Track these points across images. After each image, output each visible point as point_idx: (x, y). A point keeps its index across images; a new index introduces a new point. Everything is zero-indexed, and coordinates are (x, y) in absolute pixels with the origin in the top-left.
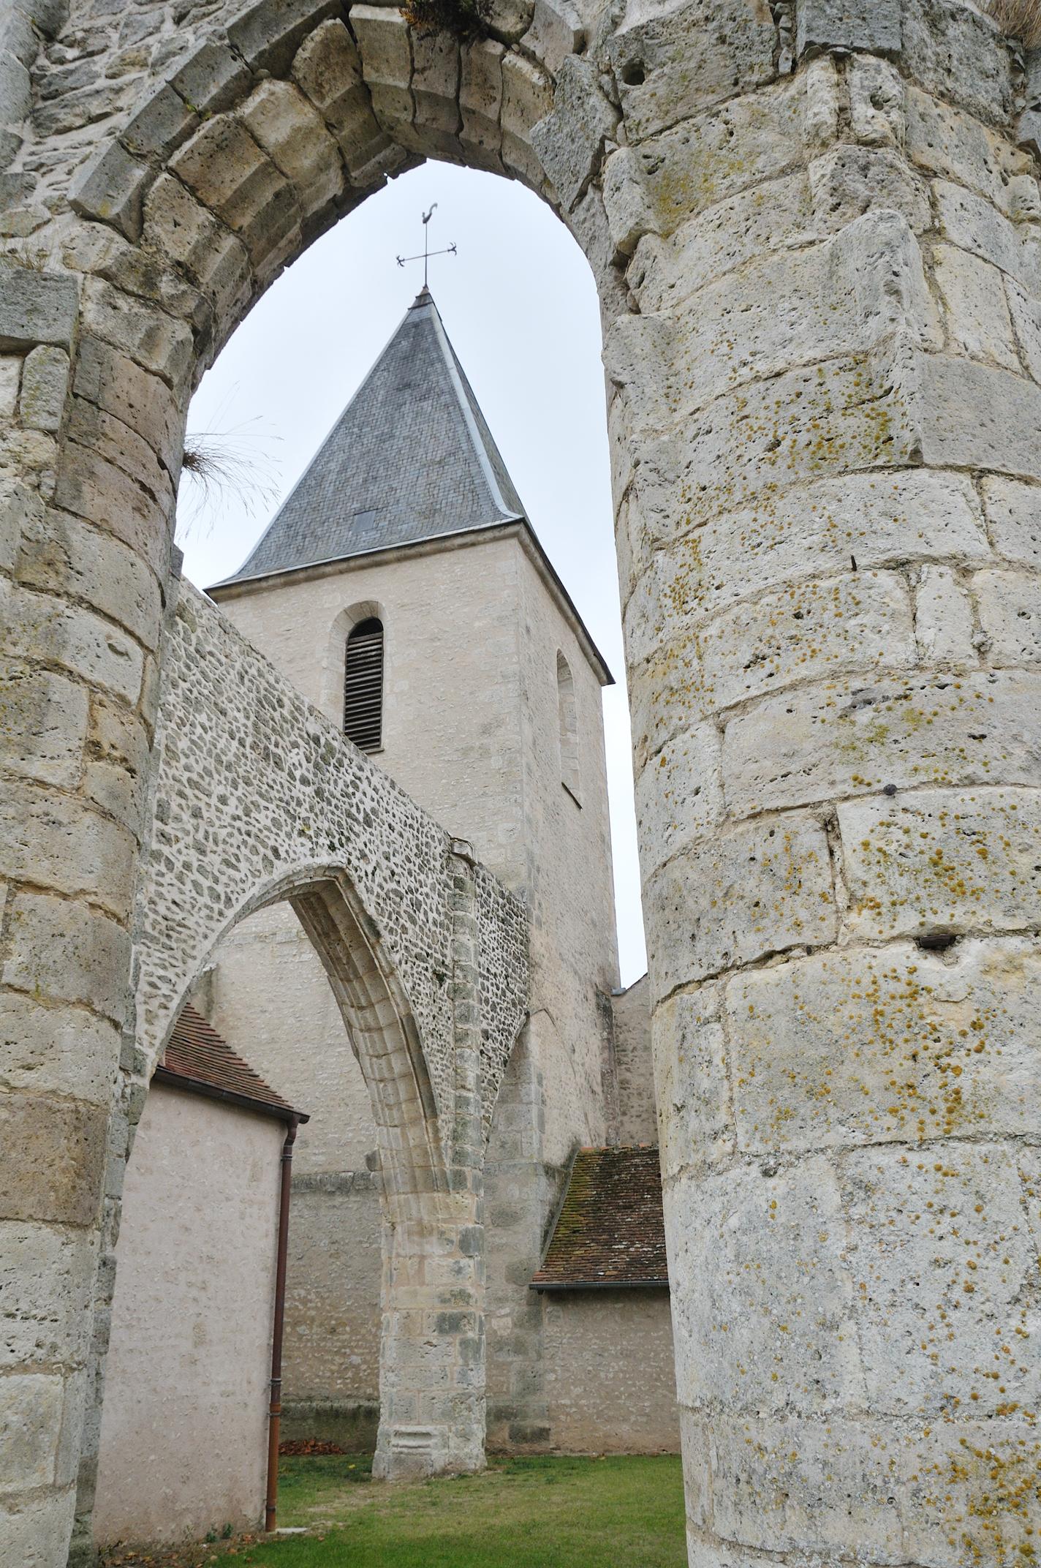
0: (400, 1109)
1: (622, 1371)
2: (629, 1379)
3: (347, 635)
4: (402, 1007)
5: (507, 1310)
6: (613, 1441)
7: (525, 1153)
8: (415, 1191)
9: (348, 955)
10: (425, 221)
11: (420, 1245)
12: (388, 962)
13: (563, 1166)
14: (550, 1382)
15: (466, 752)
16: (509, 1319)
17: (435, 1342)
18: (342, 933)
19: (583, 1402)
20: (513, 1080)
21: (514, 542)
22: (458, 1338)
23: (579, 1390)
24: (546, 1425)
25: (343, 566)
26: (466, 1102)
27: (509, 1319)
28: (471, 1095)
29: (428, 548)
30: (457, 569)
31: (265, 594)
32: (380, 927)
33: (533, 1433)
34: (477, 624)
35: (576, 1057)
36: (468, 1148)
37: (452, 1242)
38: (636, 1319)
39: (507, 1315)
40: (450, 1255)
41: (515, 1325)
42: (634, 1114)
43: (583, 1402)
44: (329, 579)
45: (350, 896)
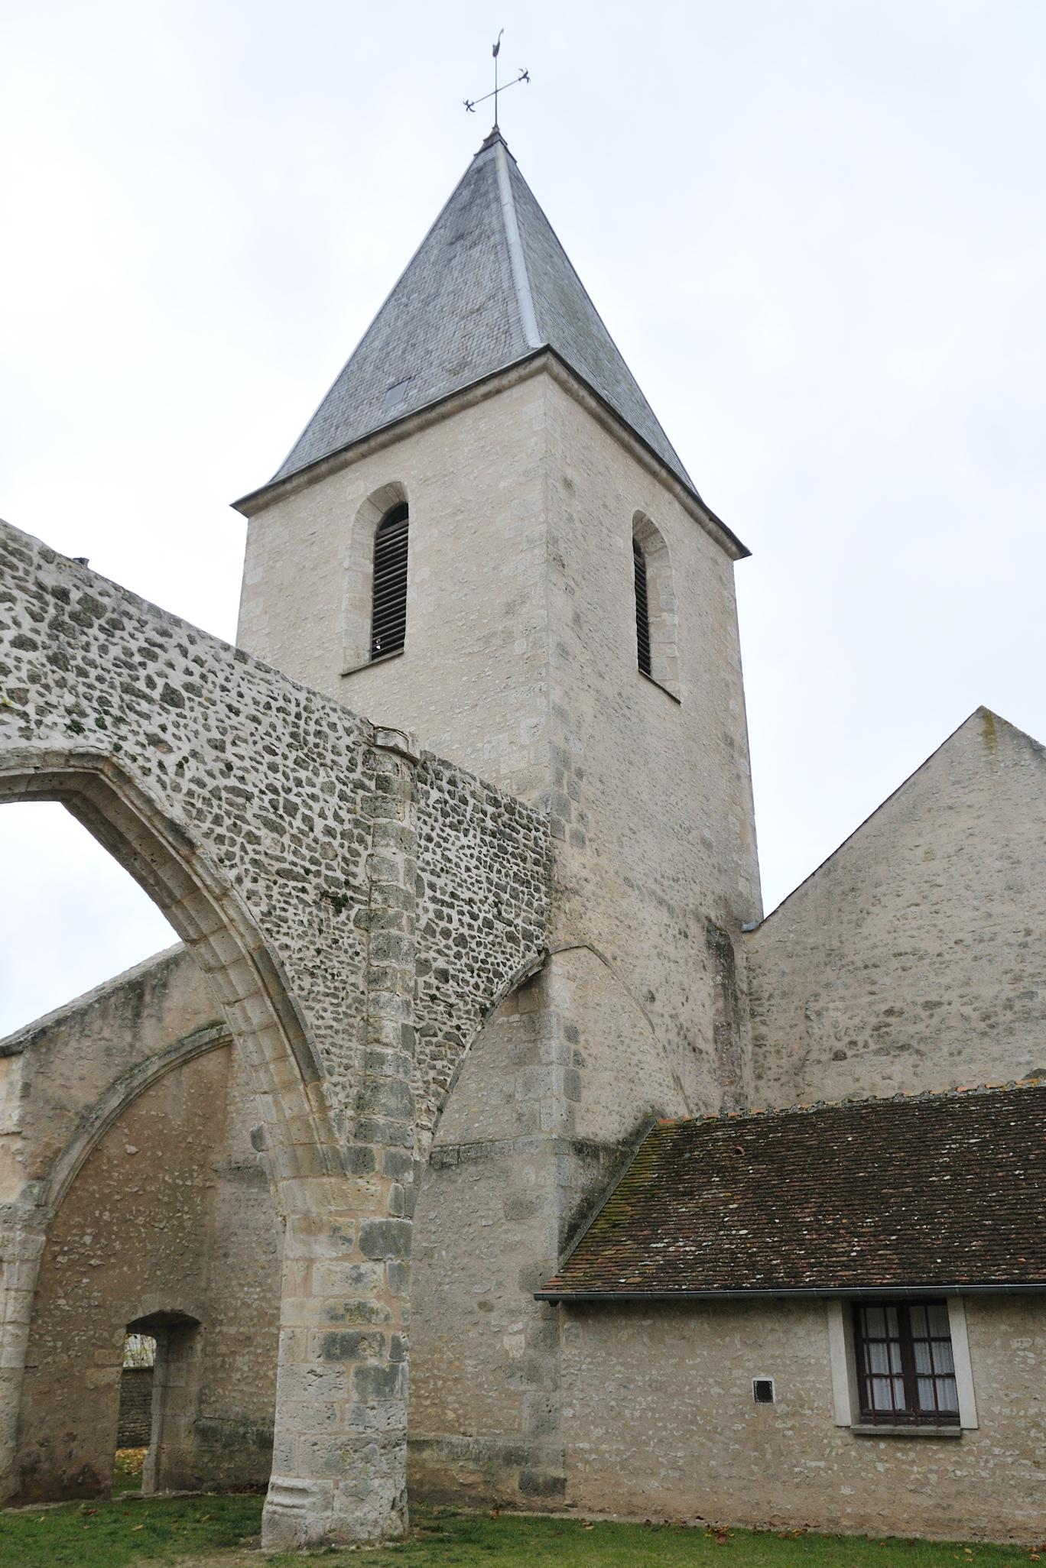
0: (267, 1071)
1: (652, 1409)
2: (659, 1419)
3: (374, 528)
4: (249, 939)
5: (520, 1326)
6: (639, 1501)
7: (544, 1127)
8: (297, 1176)
9: (156, 876)
10: (495, 53)
11: (306, 1244)
12: (215, 879)
13: (624, 1143)
14: (567, 1419)
15: (487, 640)
16: (522, 1337)
17: (319, 1371)
18: (135, 844)
19: (604, 1447)
20: (532, 1036)
21: (544, 378)
22: (353, 1365)
23: (599, 1431)
24: (560, 1473)
25: (364, 448)
26: (381, 1060)
27: (522, 1337)
28: (389, 1051)
29: (449, 406)
30: (482, 425)
31: (292, 498)
32: (194, 834)
33: (546, 1484)
34: (502, 485)
35: (657, 1006)
36: (380, 1119)
37: (350, 1241)
38: (669, 1340)
39: (520, 1332)
40: (346, 1257)
41: (528, 1345)
42: (772, 1077)
43: (604, 1447)
44: (353, 466)
45: (132, 794)
